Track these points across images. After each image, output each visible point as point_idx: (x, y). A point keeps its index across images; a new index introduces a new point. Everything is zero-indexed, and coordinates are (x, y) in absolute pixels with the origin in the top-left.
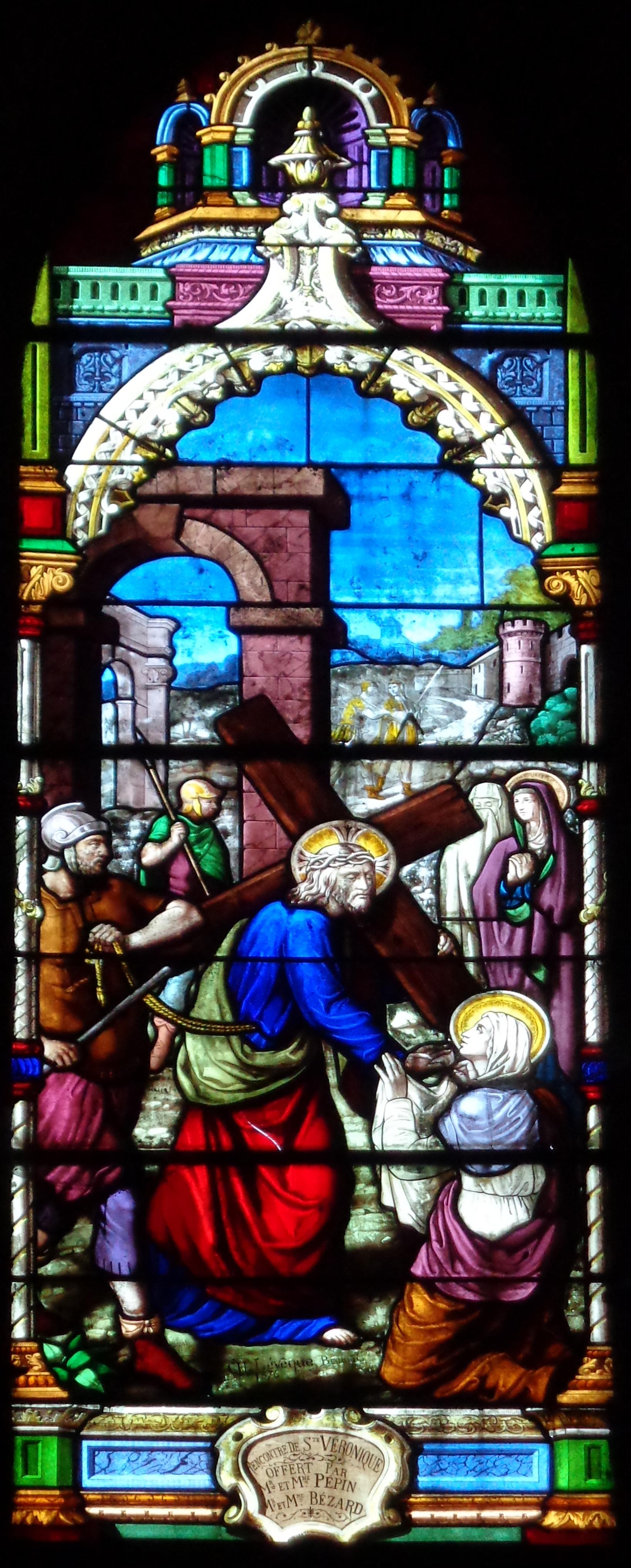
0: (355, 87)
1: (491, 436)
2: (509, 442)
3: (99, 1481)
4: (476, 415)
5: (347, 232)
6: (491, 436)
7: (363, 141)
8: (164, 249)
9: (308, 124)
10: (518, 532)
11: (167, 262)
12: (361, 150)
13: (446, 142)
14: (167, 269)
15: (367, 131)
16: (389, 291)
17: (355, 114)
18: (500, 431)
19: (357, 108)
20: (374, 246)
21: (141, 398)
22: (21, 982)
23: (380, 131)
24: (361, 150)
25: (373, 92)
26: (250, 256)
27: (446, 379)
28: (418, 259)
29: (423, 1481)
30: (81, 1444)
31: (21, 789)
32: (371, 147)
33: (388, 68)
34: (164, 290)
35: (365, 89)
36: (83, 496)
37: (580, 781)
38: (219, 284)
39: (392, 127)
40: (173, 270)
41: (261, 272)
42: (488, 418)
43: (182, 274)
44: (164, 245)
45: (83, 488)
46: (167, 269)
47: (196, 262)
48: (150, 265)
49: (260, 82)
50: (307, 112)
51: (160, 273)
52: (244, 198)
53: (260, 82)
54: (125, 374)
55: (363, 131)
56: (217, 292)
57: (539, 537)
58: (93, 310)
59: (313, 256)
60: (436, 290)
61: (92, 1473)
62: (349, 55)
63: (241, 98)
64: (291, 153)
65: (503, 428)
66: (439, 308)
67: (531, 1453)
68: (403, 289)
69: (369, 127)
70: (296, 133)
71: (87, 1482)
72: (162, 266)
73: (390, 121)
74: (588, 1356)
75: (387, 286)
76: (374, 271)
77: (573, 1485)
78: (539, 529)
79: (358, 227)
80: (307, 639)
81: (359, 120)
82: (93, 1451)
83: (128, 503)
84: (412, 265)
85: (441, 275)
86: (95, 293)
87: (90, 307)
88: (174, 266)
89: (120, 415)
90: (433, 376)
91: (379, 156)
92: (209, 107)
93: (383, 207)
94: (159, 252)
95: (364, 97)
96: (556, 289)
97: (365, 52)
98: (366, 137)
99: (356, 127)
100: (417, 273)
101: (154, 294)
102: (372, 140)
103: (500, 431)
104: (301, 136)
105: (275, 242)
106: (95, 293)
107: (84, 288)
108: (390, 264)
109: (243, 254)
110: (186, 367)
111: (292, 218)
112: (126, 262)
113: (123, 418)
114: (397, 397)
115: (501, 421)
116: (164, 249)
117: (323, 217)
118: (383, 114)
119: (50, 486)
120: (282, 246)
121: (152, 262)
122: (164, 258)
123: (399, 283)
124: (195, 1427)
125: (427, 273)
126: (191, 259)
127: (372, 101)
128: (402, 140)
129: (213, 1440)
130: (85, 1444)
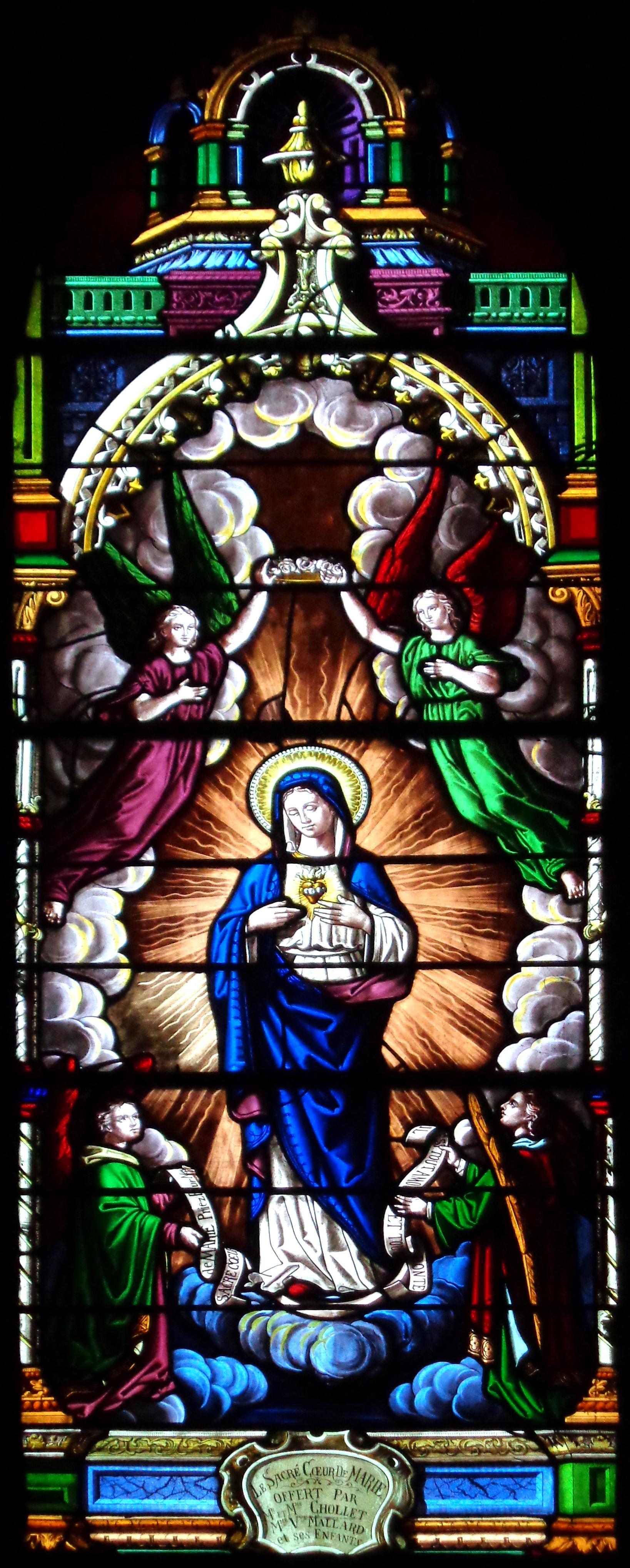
0: (351, 78)
1: (495, 437)
2: (512, 444)
3: (104, 1503)
4: (478, 417)
5: (343, 233)
6: (495, 437)
7: (359, 136)
8: (157, 257)
9: (303, 120)
10: (521, 537)
11: (161, 270)
12: (354, 145)
13: (446, 135)
14: (161, 277)
15: (363, 125)
16: (390, 296)
17: (352, 108)
18: (502, 432)
19: (355, 102)
20: (374, 247)
21: (137, 406)
22: (21, 1009)
23: (376, 124)
24: (354, 145)
25: (368, 84)
26: (245, 261)
27: (448, 380)
28: (416, 257)
29: (432, 1504)
30: (87, 1469)
31: (21, 808)
32: (368, 141)
33: (384, 59)
34: (158, 300)
35: (361, 79)
36: (80, 508)
37: (585, 794)
38: (214, 291)
39: (389, 119)
40: (166, 278)
41: (257, 278)
42: (490, 418)
43: (178, 282)
44: (158, 252)
45: (79, 499)
46: (161, 277)
47: (189, 269)
48: (143, 273)
49: (255, 75)
50: (302, 107)
51: (153, 281)
52: (239, 197)
53: (255, 75)
54: (119, 384)
55: (359, 125)
56: (212, 299)
57: (541, 542)
58: (86, 322)
59: (310, 260)
60: (437, 290)
61: (97, 1496)
62: (344, 49)
63: (235, 97)
64: (287, 150)
65: (506, 429)
66: (441, 309)
67: (534, 1475)
68: (403, 292)
69: (366, 120)
70: (292, 130)
71: (92, 1505)
72: (155, 274)
73: (387, 113)
74: (596, 1378)
75: (388, 290)
76: (375, 274)
77: (581, 1508)
78: (543, 534)
79: (355, 229)
80: (90, 1510)
81: (357, 113)
82: (98, 1475)
83: (123, 515)
84: (411, 265)
85: (442, 275)
86: (88, 304)
87: (82, 318)
88: (169, 273)
89: (115, 425)
90: (434, 376)
91: (375, 151)
92: (202, 104)
93: (382, 205)
94: (152, 259)
95: (361, 88)
96: (560, 289)
97: (360, 43)
98: (362, 131)
99: (354, 119)
100: (420, 274)
101: (148, 305)
102: (369, 133)
103: (502, 432)
104: (296, 132)
105: (270, 245)
106: (88, 304)
107: (77, 299)
108: (390, 266)
109: (236, 260)
110: (182, 371)
111: (288, 219)
112: (123, 270)
113: (119, 427)
114: (398, 400)
115: (504, 423)
116: (157, 257)
117: (319, 217)
118: (379, 105)
119: (50, 499)
120: (276, 249)
121: (145, 269)
122: (158, 265)
123: (400, 285)
124: (201, 1450)
125: (426, 274)
126: (184, 266)
127: (369, 93)
128: (400, 131)
129: (218, 1464)
130: (91, 1469)
